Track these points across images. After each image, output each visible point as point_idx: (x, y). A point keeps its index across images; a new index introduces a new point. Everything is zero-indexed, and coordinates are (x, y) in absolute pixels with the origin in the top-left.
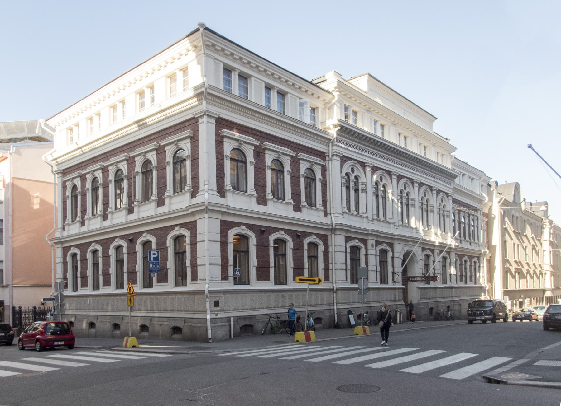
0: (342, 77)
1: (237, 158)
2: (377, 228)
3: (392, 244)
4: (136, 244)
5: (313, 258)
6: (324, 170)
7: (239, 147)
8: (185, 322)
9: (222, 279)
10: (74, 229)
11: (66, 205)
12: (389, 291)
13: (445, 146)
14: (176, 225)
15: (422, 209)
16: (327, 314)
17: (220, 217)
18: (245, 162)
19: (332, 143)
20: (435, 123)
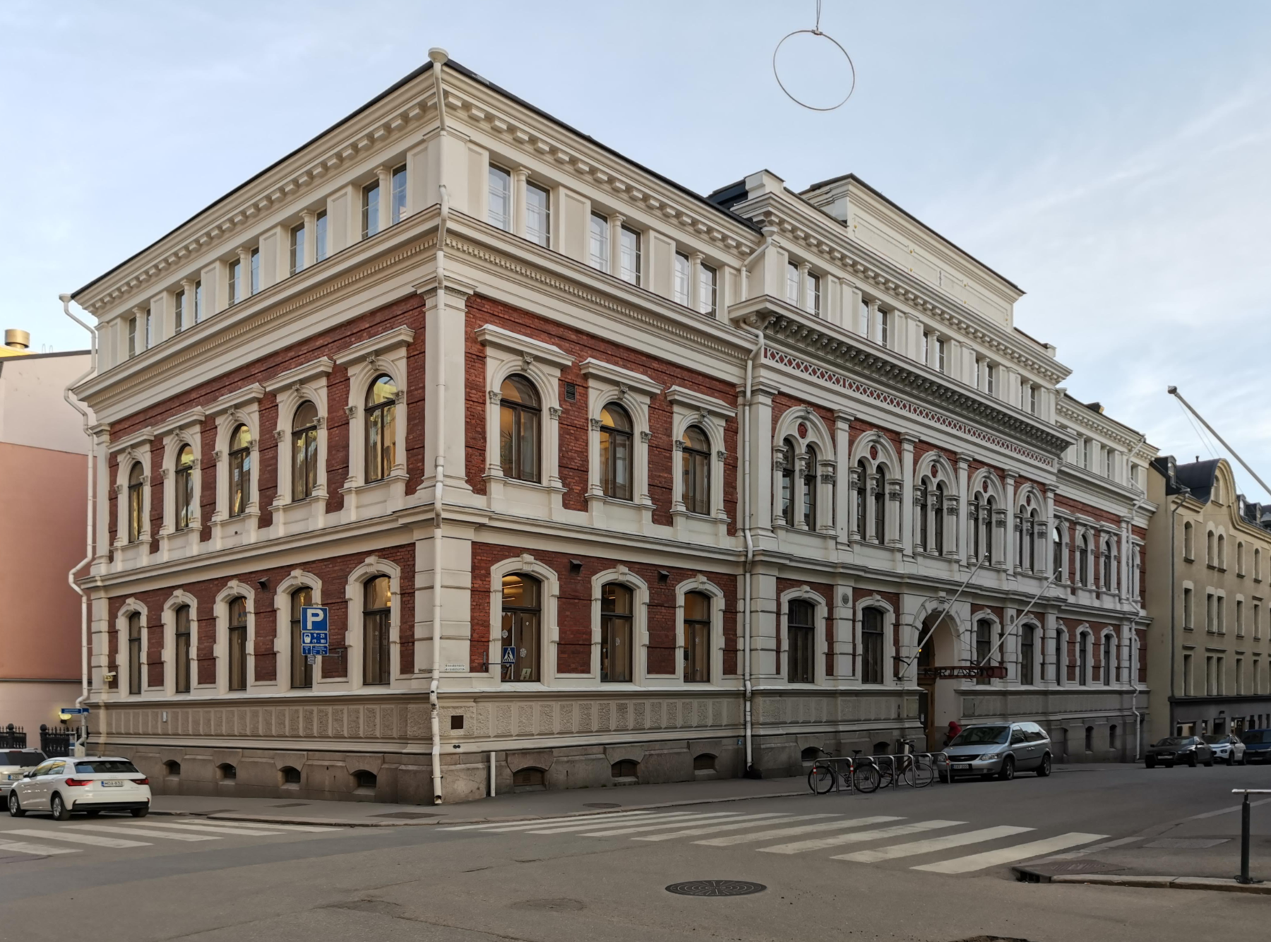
0: (785, 185)
1: (520, 401)
2: (859, 561)
3: (1043, 614)
4: (275, 593)
5: (699, 625)
6: (732, 429)
7: (523, 370)
8: (384, 762)
9: (472, 670)
11: (116, 506)
12: (884, 699)
13: (1040, 365)
14: (369, 553)
15: (976, 520)
16: (729, 746)
17: (471, 534)
18: (537, 411)
19: (754, 360)
20: (1020, 305)
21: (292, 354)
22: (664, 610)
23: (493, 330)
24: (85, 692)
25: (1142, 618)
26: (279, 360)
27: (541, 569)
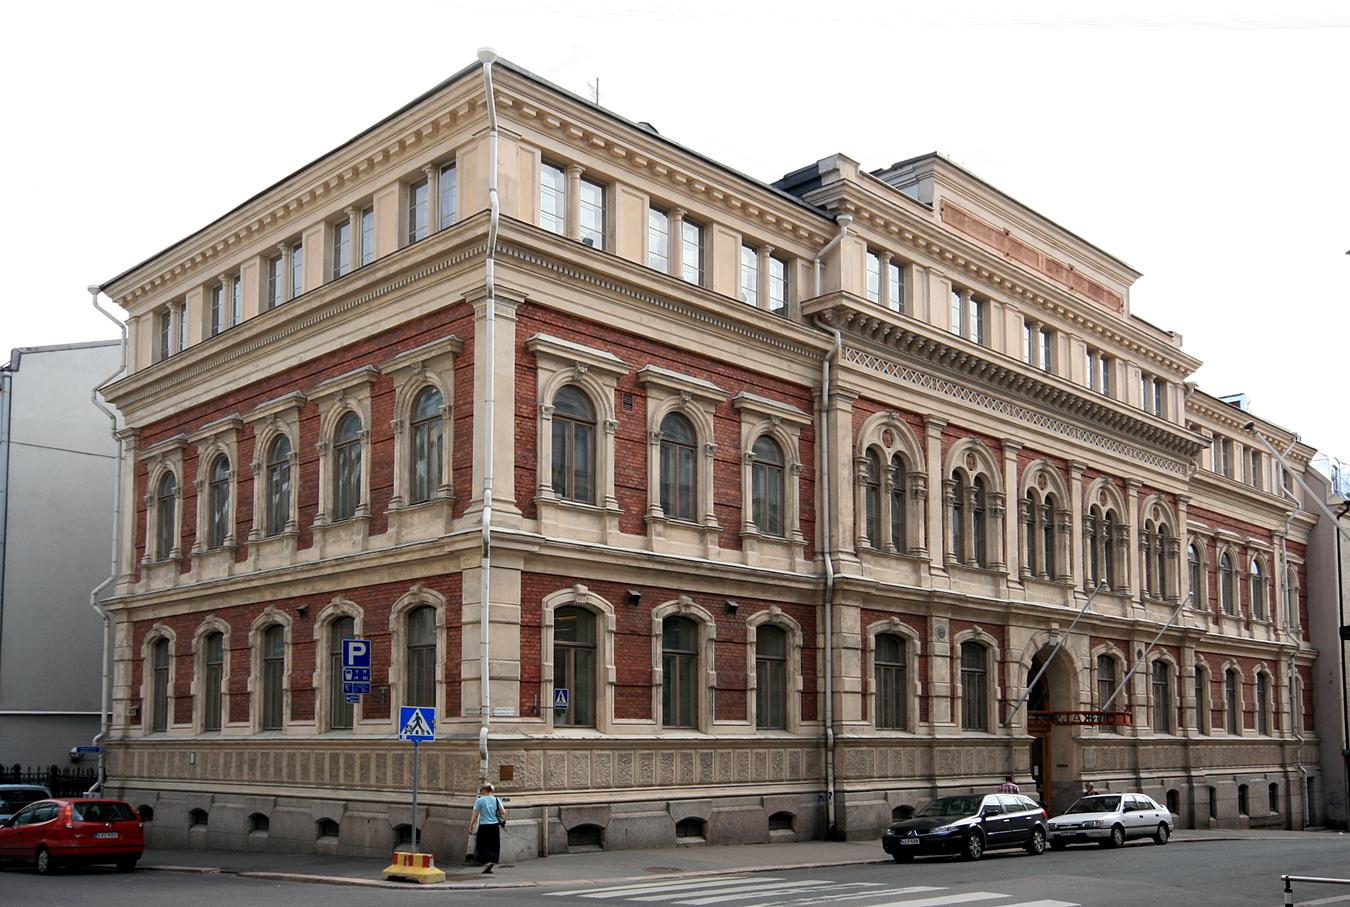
6: (809, 437)
9: (522, 714)
10: (162, 581)
13: (1164, 362)
21: (335, 361)
22: (733, 647)
23: (547, 339)
24: (104, 729)
25: (1303, 652)
26: (322, 366)
27: (596, 600)
